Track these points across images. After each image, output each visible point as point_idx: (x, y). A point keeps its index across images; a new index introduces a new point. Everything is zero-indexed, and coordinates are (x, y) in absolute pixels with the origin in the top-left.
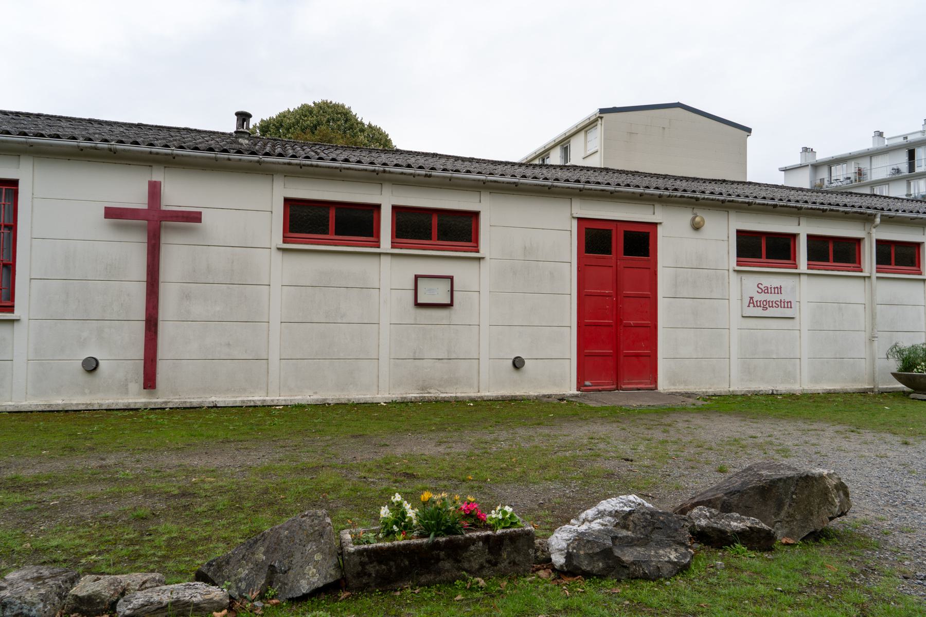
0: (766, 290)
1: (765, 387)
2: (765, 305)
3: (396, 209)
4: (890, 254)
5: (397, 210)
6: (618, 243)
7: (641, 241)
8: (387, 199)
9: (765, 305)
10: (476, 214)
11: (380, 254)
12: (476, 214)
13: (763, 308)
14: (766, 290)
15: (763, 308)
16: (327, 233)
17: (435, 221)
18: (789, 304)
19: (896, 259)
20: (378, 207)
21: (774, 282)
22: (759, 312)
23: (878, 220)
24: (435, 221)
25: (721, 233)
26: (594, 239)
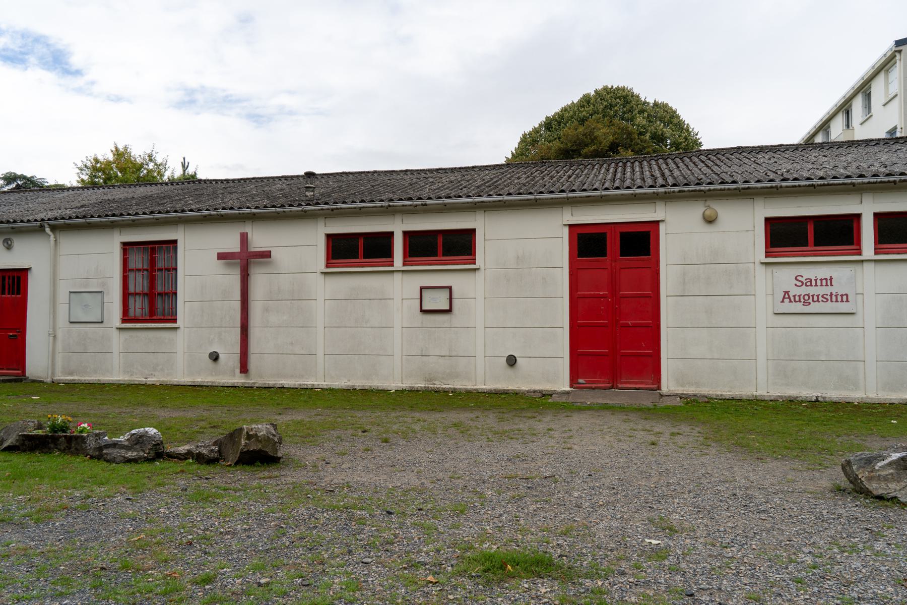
6: (613, 244)
7: (641, 242)
8: (398, 227)
10: (473, 231)
11: (393, 272)
12: (473, 231)
18: (845, 298)
26: (587, 243)
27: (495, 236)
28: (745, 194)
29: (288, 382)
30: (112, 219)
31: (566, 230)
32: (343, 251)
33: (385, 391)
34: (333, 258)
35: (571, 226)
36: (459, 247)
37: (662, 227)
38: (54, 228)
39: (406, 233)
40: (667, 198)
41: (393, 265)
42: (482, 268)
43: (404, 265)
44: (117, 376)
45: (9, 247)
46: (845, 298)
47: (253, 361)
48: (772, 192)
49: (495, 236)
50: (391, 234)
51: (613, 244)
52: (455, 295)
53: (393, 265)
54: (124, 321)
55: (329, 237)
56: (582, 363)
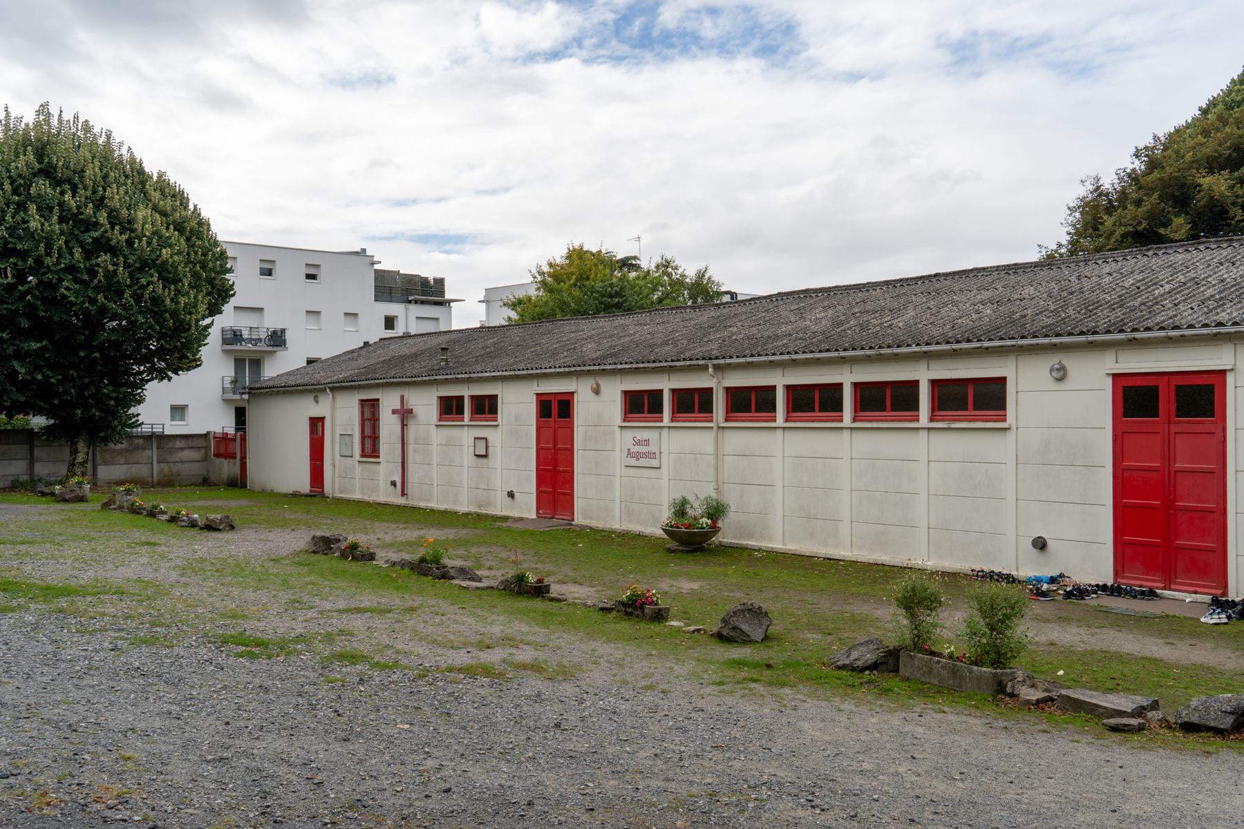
0: (638, 443)
1: (635, 528)
2: (638, 456)
3: (934, 383)
4: (693, 402)
5: (789, 388)
6: (1166, 402)
7: (1201, 398)
8: (924, 375)
9: (638, 456)
10: (1002, 381)
11: (918, 429)
12: (1002, 381)
13: (640, 457)
14: (638, 443)
15: (640, 457)
16: (967, 409)
17: (970, 392)
18: (652, 455)
19: (757, 404)
20: (916, 383)
21: (643, 435)
22: (633, 462)
23: (711, 370)
24: (970, 392)
25: (613, 391)
26: (1135, 398)
27: (1027, 382)
28: (1091, 343)
29: (422, 505)
30: (688, 363)
31: (1109, 381)
32: (640, 406)
33: (456, 513)
34: (733, 411)
35: (1116, 377)
36: (987, 399)
37: (1230, 379)
38: (332, 389)
39: (934, 383)
40: (577, 374)
41: (1005, 420)
42: (1014, 427)
43: (787, 421)
44: (357, 496)
45: (317, 402)
46: (652, 455)
47: (410, 489)
48: (360, 388)
49: (1027, 382)
50: (840, 386)
51: (1166, 402)
52: (490, 444)
53: (1005, 420)
54: (363, 456)
55: (626, 393)
56: (1124, 555)
